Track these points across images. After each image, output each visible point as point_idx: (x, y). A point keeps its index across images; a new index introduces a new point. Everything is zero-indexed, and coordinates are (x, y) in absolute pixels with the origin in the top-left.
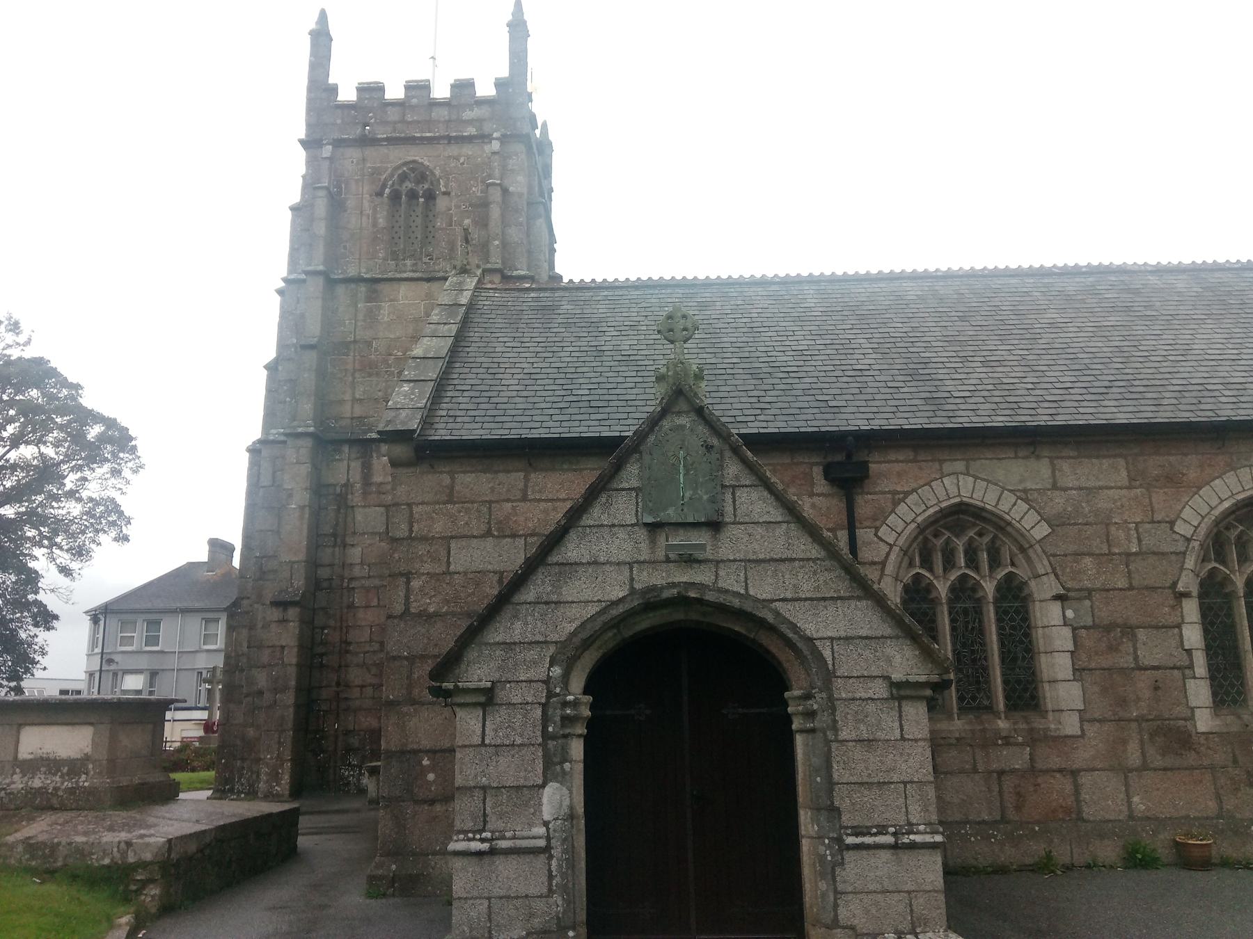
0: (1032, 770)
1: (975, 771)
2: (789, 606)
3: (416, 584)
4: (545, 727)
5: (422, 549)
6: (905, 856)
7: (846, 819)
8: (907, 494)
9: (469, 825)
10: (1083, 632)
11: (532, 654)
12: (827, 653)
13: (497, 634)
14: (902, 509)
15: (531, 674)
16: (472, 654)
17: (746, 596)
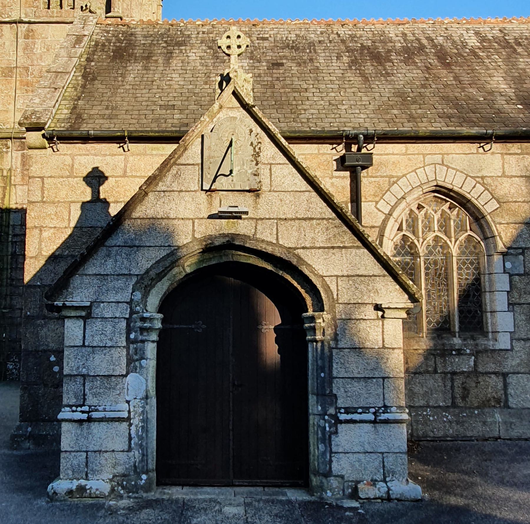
0: (475, 372)
1: (435, 371)
2: (308, 252)
3: (45, 234)
4: (128, 333)
5: (51, 209)
6: (381, 428)
7: (341, 403)
8: (399, 178)
9: (73, 401)
10: (517, 278)
11: (120, 283)
12: (333, 287)
13: (92, 268)
14: (395, 188)
15: (119, 298)
16: (76, 281)
17: (278, 245)
